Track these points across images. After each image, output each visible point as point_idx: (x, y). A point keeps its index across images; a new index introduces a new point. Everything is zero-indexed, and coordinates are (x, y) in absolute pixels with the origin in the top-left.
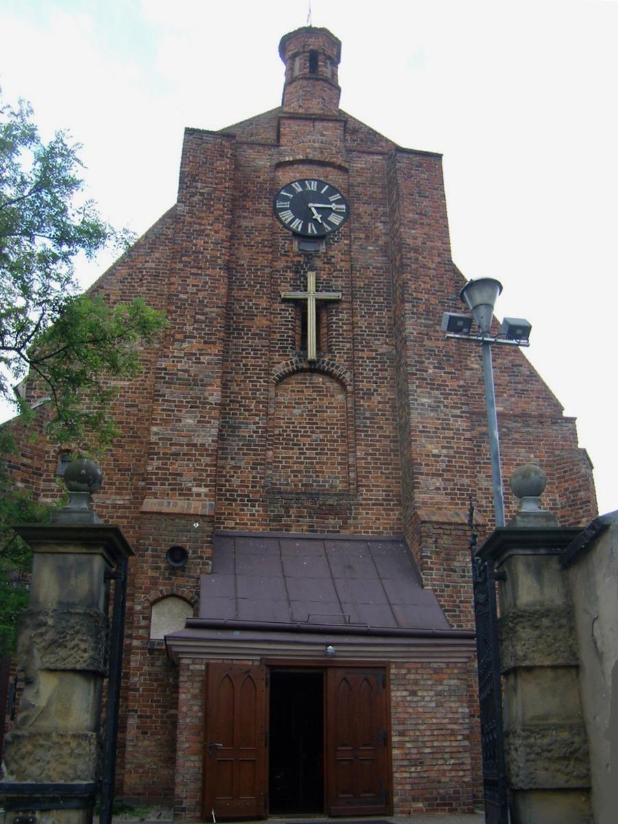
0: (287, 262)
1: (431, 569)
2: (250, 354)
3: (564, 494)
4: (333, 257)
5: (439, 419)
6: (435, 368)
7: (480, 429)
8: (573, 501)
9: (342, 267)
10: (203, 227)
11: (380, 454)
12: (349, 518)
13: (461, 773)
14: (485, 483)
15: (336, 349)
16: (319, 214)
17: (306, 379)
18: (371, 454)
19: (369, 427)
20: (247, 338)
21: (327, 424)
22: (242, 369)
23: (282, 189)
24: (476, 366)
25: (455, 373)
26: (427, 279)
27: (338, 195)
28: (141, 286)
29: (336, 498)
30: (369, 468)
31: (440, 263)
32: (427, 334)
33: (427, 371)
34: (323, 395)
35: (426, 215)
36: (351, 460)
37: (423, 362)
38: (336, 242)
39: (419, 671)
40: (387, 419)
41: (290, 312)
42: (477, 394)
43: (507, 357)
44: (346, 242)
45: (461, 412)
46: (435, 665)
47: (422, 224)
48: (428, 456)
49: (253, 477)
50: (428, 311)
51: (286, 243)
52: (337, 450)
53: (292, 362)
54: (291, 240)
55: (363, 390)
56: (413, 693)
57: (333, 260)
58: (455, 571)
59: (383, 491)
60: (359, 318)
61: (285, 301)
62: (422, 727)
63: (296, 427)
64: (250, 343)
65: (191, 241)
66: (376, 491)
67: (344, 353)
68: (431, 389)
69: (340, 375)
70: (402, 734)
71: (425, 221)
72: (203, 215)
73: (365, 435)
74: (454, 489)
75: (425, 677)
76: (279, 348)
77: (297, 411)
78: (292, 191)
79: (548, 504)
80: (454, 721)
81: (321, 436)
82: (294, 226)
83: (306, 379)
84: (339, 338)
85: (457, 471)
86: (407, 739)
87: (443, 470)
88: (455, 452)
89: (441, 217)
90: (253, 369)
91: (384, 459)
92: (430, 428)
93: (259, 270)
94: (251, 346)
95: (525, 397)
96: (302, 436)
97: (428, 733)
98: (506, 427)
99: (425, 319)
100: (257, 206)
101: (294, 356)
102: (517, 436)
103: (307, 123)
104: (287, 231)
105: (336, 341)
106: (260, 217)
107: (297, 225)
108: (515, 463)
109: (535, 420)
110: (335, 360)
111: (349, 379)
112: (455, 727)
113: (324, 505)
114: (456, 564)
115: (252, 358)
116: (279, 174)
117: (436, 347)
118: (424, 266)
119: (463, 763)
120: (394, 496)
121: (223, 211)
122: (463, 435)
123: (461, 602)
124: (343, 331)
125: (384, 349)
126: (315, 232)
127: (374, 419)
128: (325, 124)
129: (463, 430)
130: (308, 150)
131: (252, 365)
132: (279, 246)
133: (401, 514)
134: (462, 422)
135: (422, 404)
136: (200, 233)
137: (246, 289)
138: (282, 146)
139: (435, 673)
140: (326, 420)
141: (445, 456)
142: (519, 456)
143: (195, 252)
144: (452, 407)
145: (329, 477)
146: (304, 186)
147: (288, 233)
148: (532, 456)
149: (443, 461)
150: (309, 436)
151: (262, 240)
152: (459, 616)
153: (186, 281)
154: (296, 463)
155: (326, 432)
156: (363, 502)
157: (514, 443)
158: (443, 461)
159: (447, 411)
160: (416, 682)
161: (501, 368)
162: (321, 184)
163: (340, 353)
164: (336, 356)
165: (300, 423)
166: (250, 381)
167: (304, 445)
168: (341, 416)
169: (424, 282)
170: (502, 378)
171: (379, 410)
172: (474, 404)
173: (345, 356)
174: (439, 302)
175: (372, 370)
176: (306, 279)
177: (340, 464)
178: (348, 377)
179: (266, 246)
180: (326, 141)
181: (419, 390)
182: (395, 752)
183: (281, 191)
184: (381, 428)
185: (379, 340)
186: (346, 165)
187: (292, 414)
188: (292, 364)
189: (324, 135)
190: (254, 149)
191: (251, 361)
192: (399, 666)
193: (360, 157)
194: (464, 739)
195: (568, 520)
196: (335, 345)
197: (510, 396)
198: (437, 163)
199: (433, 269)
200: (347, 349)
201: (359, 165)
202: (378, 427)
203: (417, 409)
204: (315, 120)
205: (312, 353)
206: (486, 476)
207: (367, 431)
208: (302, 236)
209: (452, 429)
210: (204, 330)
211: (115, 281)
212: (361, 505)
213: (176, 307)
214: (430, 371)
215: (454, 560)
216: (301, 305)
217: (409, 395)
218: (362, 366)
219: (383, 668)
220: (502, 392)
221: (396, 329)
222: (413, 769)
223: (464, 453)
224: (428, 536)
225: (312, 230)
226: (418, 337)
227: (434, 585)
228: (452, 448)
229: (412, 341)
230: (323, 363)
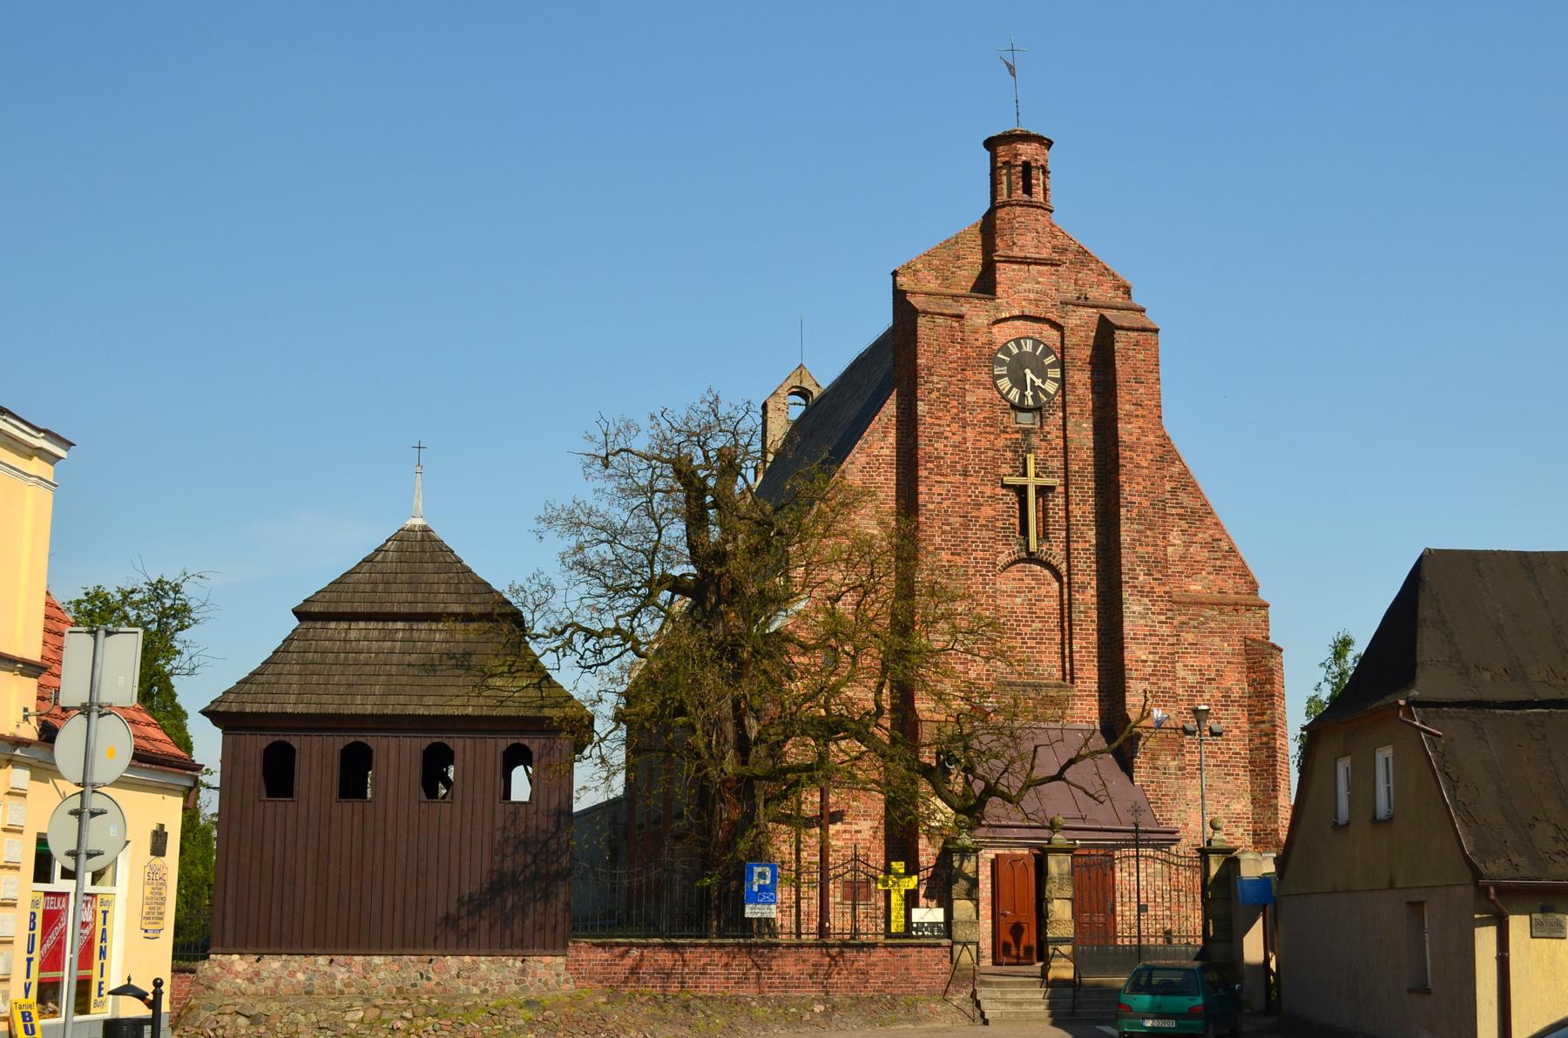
0: (1006, 439)
1: (1140, 768)
2: (978, 546)
4: (1049, 433)
5: (1147, 626)
6: (1145, 574)
8: (1260, 692)
12: (1066, 709)
15: (1053, 538)
16: (1038, 378)
17: (1026, 567)
18: (1085, 648)
19: (1084, 621)
20: (976, 530)
21: (1045, 613)
22: (972, 563)
25: (1161, 579)
26: (1140, 480)
27: (1053, 356)
28: (879, 475)
29: (1055, 689)
30: (1083, 661)
31: (1152, 460)
32: (1139, 540)
33: (1138, 579)
34: (1041, 584)
35: (1141, 405)
38: (1051, 414)
41: (1012, 497)
43: (1208, 531)
45: (1166, 618)
47: (1137, 416)
48: (1137, 661)
49: (987, 670)
50: (1140, 515)
51: (1004, 417)
54: (1009, 414)
55: (1078, 583)
58: (1158, 769)
60: (1074, 506)
63: (1018, 616)
64: (978, 535)
65: (933, 445)
66: (1089, 683)
68: (1142, 596)
69: (1057, 565)
72: (940, 414)
73: (1080, 629)
74: (1158, 692)
76: (1003, 536)
77: (1018, 600)
78: (1007, 352)
82: (1011, 396)
83: (1026, 567)
84: (1055, 525)
85: (1162, 675)
87: (1150, 675)
88: (1160, 657)
90: (982, 563)
92: (1140, 635)
93: (983, 453)
94: (979, 538)
95: (1223, 574)
96: (1023, 626)
98: (1203, 616)
99: (1138, 524)
100: (978, 377)
102: (1212, 625)
103: (1023, 266)
104: (1004, 402)
105: (1053, 529)
106: (981, 390)
107: (1014, 395)
108: (1210, 652)
109: (1231, 608)
110: (1051, 550)
116: (995, 329)
117: (1147, 553)
118: (1138, 466)
121: (958, 408)
123: (1162, 795)
124: (1059, 517)
127: (1087, 613)
128: (1040, 268)
129: (1168, 636)
130: (1024, 303)
132: (997, 420)
133: (1109, 705)
135: (1134, 613)
136: (939, 435)
137: (972, 476)
138: (998, 298)
142: (1214, 645)
143: (936, 458)
144: (1158, 614)
145: (1047, 666)
146: (1019, 346)
147: (1006, 405)
149: (1149, 666)
150: (1030, 626)
151: (984, 418)
152: (1161, 807)
153: (931, 490)
157: (1210, 632)
158: (1149, 666)
162: (1037, 343)
163: (1056, 542)
166: (980, 575)
169: (1138, 484)
170: (1202, 554)
172: (1174, 583)
174: (1151, 504)
175: (1086, 563)
178: (1063, 568)
179: (988, 425)
180: (1041, 291)
181: (1132, 598)
183: (997, 354)
186: (1059, 321)
187: (1014, 603)
188: (1014, 553)
189: (1038, 283)
191: (980, 554)
193: (1075, 311)
195: (1255, 710)
196: (1052, 533)
197: (1209, 573)
198: (1153, 338)
199: (1146, 468)
201: (1074, 322)
202: (1091, 621)
205: (1033, 546)
206: (1184, 666)
207: (1082, 625)
208: (1019, 408)
211: (855, 470)
214: (1141, 578)
216: (1021, 491)
218: (1077, 558)
220: (1202, 570)
223: (1167, 658)
226: (1131, 544)
227: (1142, 781)
228: (1157, 653)
229: (1125, 548)
230: (1041, 553)
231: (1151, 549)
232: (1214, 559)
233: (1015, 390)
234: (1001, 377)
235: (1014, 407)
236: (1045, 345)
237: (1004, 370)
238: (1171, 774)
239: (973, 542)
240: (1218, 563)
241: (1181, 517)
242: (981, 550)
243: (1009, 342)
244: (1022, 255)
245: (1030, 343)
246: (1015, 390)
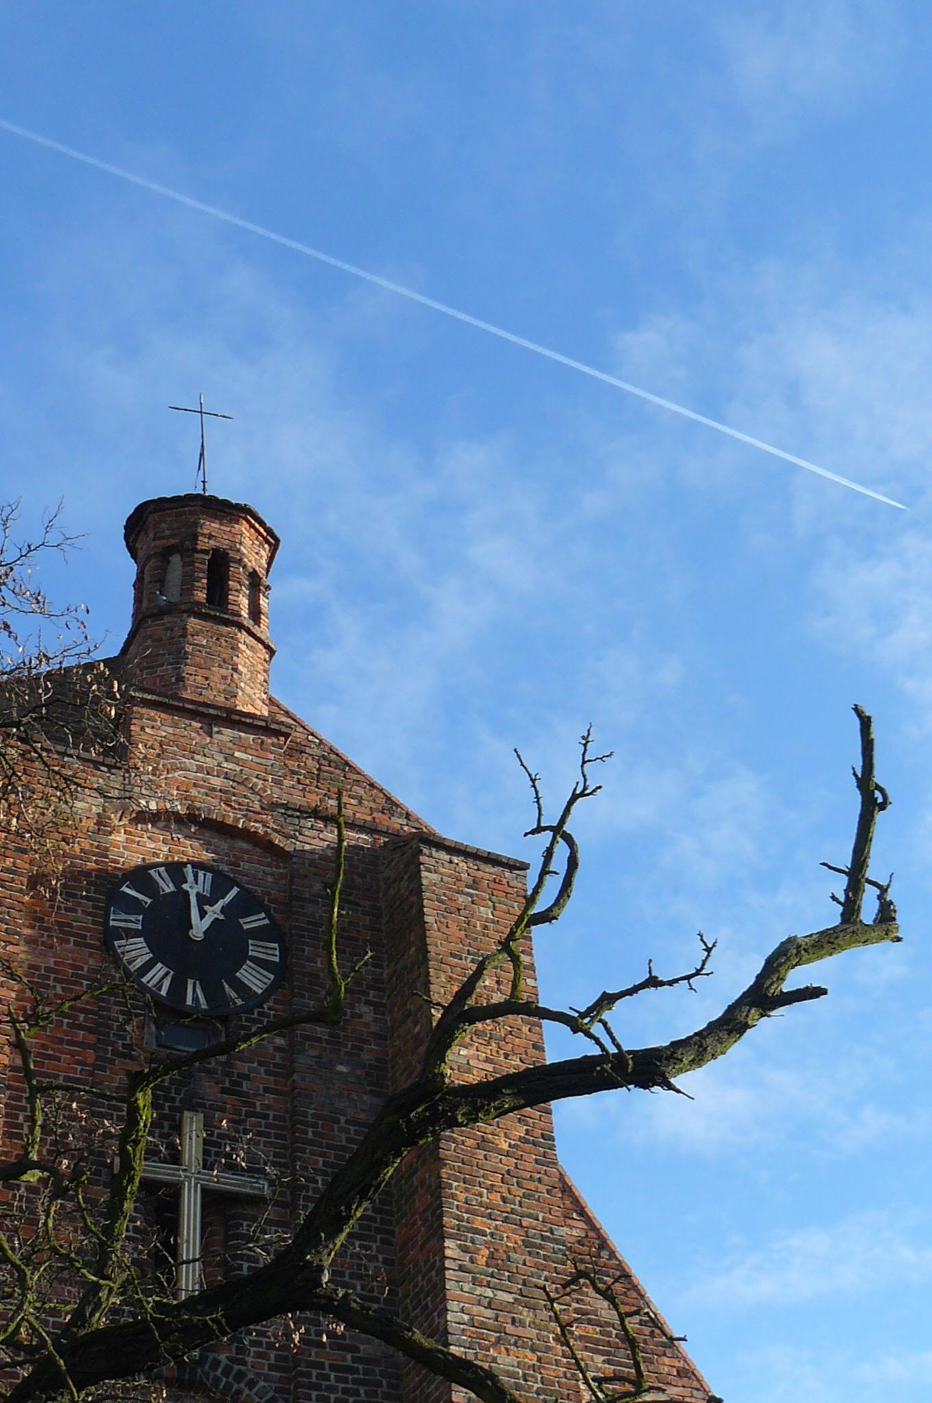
9: (268, 1107)
57: (246, 1086)
126: (204, 1004)
173: (272, 1354)
225: (196, 999)
233: (159, 970)
234: (119, 933)
237: (136, 922)
246: (159, 970)
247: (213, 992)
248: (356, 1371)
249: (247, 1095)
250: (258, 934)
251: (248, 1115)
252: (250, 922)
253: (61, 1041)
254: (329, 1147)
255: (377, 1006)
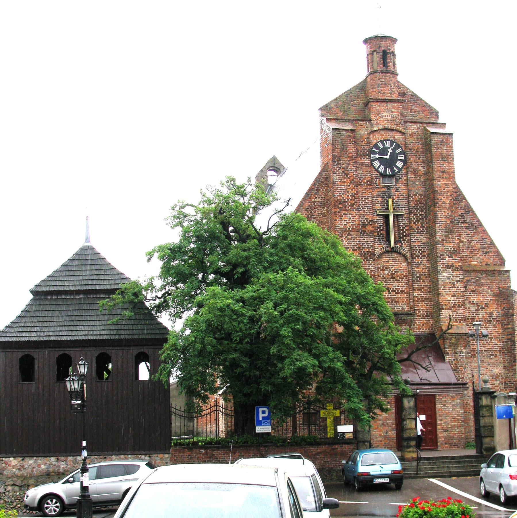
0: (378, 191)
3: (503, 310)
6: (449, 257)
7: (466, 278)
9: (404, 193)
10: (346, 188)
11: (424, 294)
13: (461, 434)
14: (469, 305)
15: (403, 240)
23: (373, 146)
24: (465, 240)
25: (457, 259)
30: (419, 301)
31: (451, 200)
33: (445, 259)
34: (397, 263)
36: (411, 297)
37: (444, 255)
39: (447, 397)
40: (426, 277)
42: (465, 255)
44: (405, 178)
46: (452, 395)
48: (446, 300)
52: (404, 291)
53: (383, 248)
56: (444, 405)
59: (425, 312)
61: (378, 215)
62: (447, 418)
67: (407, 242)
68: (447, 268)
69: (405, 254)
70: (441, 420)
71: (445, 175)
75: (449, 399)
77: (386, 272)
79: (496, 314)
80: (458, 416)
81: (397, 284)
82: (380, 170)
83: (389, 255)
85: (458, 307)
86: (443, 422)
89: (452, 172)
91: (426, 297)
92: (447, 287)
94: (366, 242)
96: (389, 285)
97: (450, 420)
101: (384, 244)
103: (384, 103)
105: (402, 236)
108: (482, 295)
111: (409, 256)
112: (459, 418)
113: (401, 319)
114: (457, 350)
115: (367, 248)
118: (444, 203)
119: (462, 431)
120: (430, 314)
122: (460, 290)
125: (424, 240)
126: (390, 173)
127: (420, 277)
129: (460, 287)
131: (367, 252)
134: (460, 283)
135: (444, 276)
136: (345, 191)
139: (452, 398)
140: (399, 276)
141: (453, 300)
146: (383, 144)
147: (377, 174)
148: (489, 291)
149: (452, 303)
150: (392, 285)
154: (387, 298)
155: (399, 282)
156: (417, 317)
158: (452, 303)
159: (454, 278)
160: (445, 401)
161: (476, 240)
164: (402, 244)
165: (388, 278)
167: (390, 289)
168: (405, 274)
169: (444, 212)
171: (423, 273)
173: (407, 244)
174: (451, 222)
176: (388, 201)
177: (406, 298)
178: (408, 255)
182: (439, 427)
184: (424, 281)
185: (422, 236)
186: (403, 131)
188: (384, 249)
190: (359, 123)
192: (439, 395)
194: (462, 422)
196: (402, 238)
197: (481, 255)
199: (448, 204)
200: (408, 240)
203: (441, 279)
204: (387, 102)
205: (393, 245)
208: (383, 175)
209: (456, 287)
210: (351, 244)
212: (416, 319)
213: (339, 233)
214: (447, 259)
215: (457, 349)
216: (387, 217)
217: (438, 272)
219: (434, 396)
221: (432, 235)
222: (445, 433)
223: (461, 298)
224: (447, 339)
231: (452, 245)
232: (483, 248)
233: (382, 167)
235: (381, 175)
236: (396, 143)
238: (463, 356)
239: (363, 244)
240: (485, 250)
241: (466, 228)
242: (367, 248)
243: (378, 142)
244: (384, 98)
245: (389, 142)
246: (382, 167)
247: (392, 170)
248: (421, 246)
249: (399, 191)
250: (400, 153)
251: (400, 196)
252: (397, 151)
253: (365, 189)
254: (416, 201)
255: (423, 167)
